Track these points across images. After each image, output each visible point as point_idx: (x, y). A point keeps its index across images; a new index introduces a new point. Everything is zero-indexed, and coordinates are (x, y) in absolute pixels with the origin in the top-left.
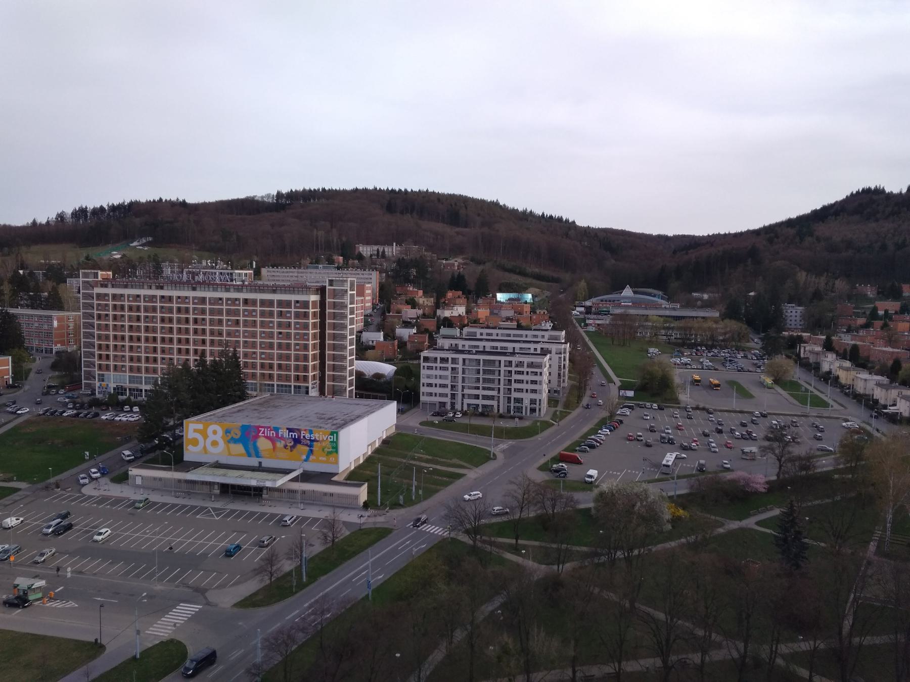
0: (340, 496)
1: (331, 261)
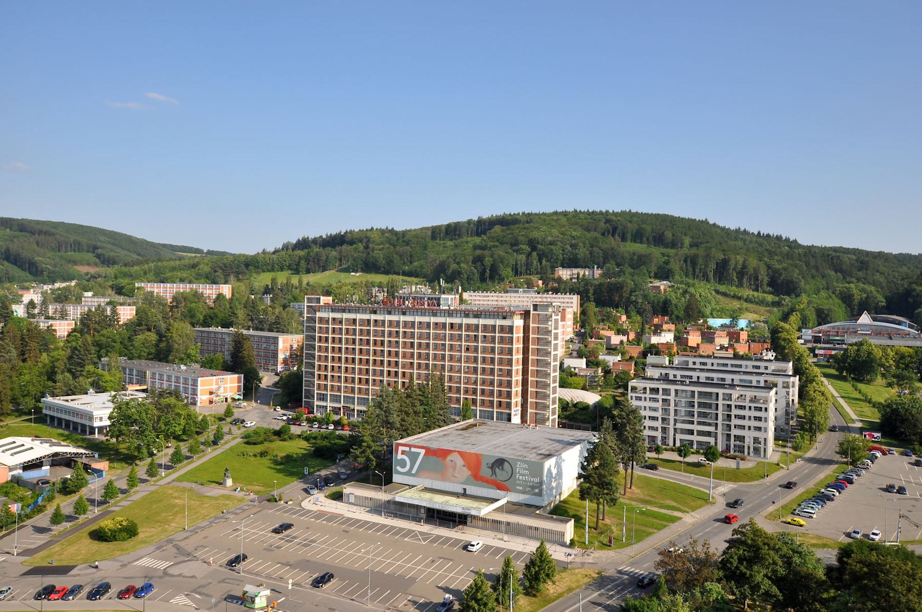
0: (544, 530)
1: (530, 285)
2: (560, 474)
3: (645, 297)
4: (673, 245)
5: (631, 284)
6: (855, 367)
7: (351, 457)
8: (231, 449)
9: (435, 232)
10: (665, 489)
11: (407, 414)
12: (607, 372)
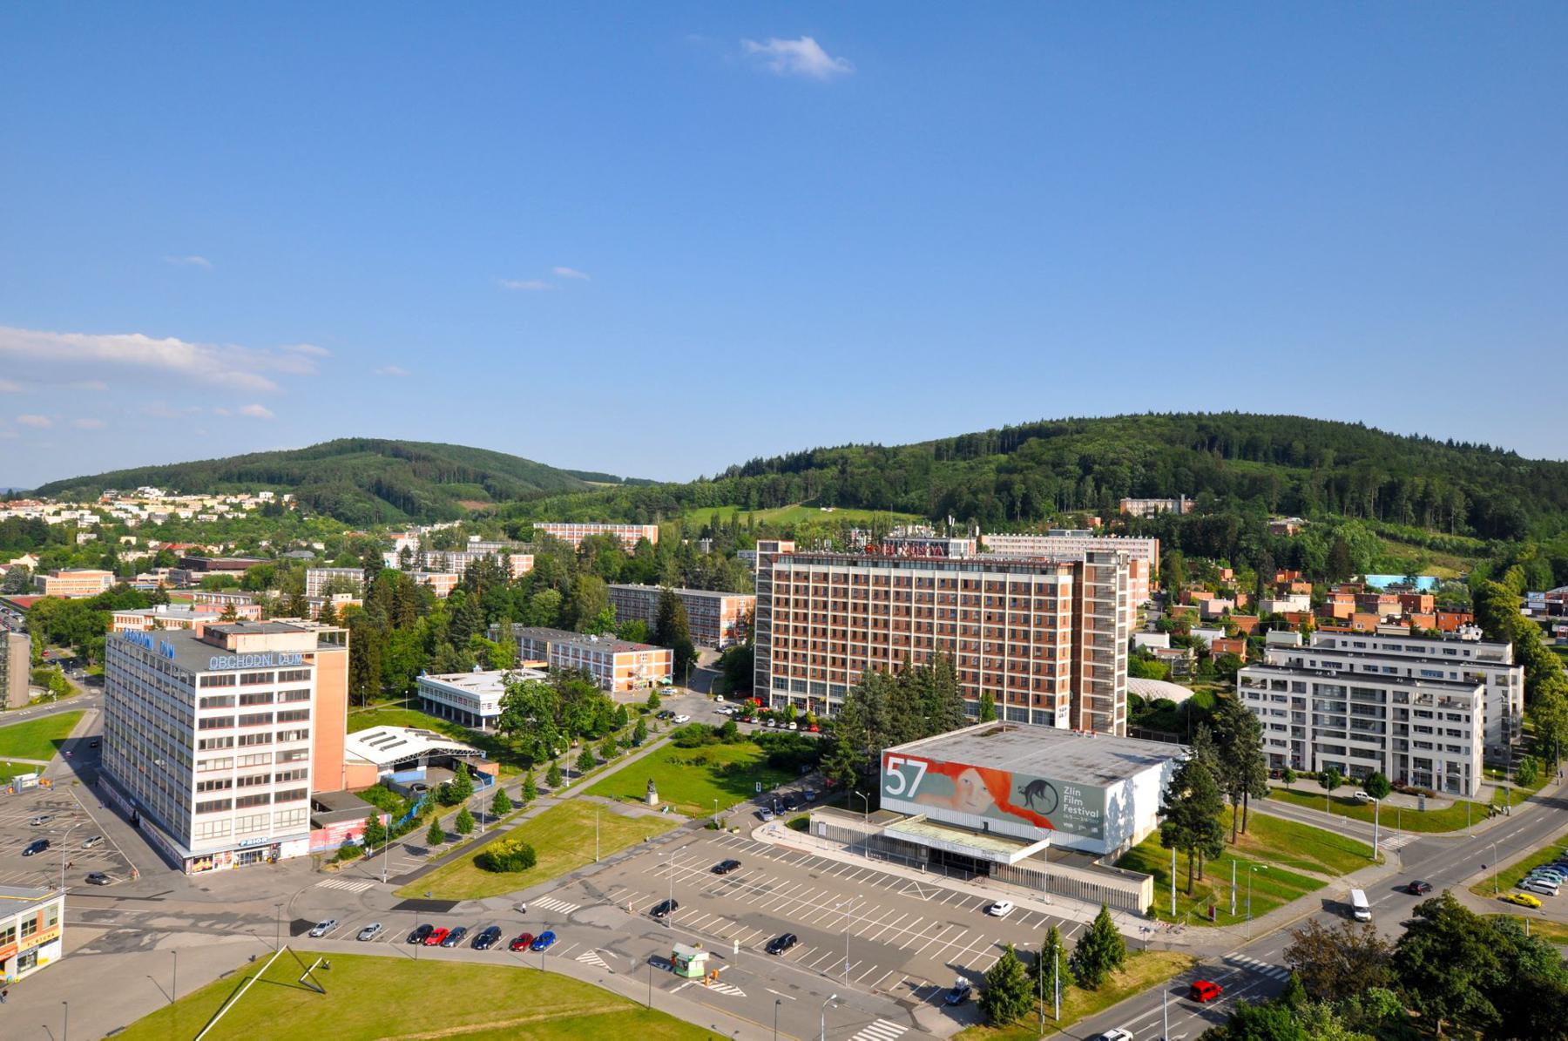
1: (1082, 524)
2: (1130, 807)
4: (1307, 462)
7: (821, 770)
8: (657, 753)
10: (1299, 837)
11: (901, 711)
12: (1203, 654)
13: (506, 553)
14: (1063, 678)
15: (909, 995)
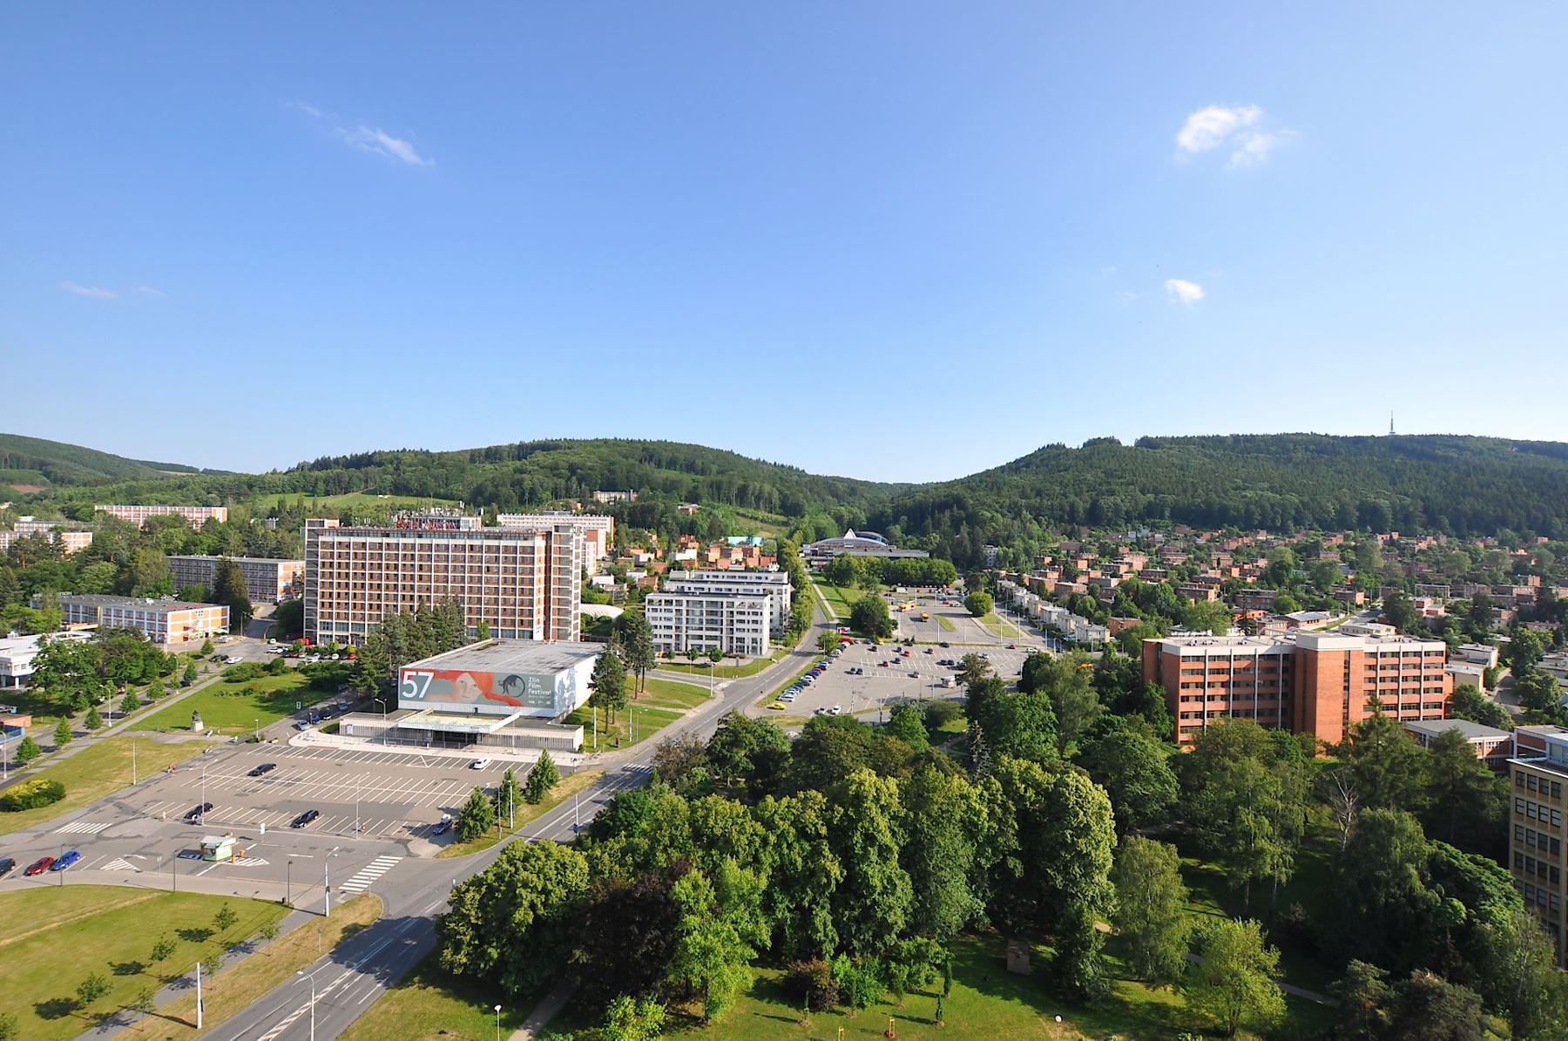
1: (568, 508)
2: (572, 685)
3: (674, 518)
4: (703, 472)
5: (662, 507)
6: (837, 575)
7: (355, 687)
8: (206, 689)
9: (475, 456)
10: (673, 689)
11: (417, 638)
12: (632, 587)
13: (58, 531)
14: (539, 607)
15: (406, 835)
